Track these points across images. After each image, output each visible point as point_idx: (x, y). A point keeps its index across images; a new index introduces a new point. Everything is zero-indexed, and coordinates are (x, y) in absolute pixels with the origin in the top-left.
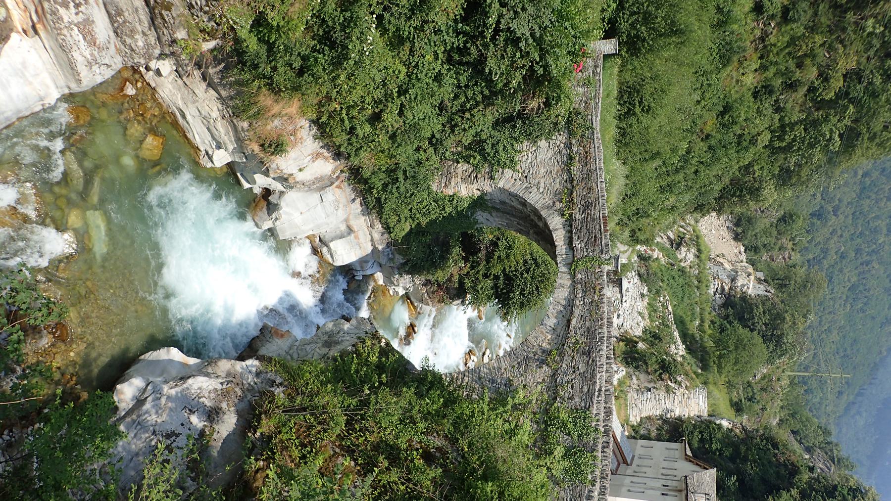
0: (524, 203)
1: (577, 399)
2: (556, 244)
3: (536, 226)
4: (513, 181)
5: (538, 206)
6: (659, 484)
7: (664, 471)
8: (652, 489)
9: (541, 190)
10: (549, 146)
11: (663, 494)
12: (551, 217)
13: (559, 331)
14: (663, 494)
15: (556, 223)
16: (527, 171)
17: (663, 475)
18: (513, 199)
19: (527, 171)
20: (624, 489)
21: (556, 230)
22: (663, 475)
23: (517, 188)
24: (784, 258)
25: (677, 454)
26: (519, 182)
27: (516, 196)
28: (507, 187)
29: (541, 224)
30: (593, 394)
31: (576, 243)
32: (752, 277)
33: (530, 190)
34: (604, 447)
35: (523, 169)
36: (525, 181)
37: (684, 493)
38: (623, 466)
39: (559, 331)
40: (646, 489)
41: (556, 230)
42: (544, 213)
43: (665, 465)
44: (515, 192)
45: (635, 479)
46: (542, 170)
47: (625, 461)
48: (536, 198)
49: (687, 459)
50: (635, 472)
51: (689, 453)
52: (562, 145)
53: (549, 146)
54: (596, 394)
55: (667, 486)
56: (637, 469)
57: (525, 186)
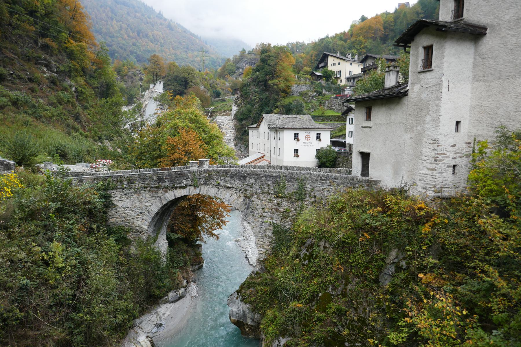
0: (157, 214)
1: (269, 183)
2: (183, 195)
3: (169, 207)
4: (143, 221)
5: (160, 206)
6: (274, 141)
7: (266, 138)
8: (277, 144)
9: (150, 204)
10: (122, 201)
11: (279, 139)
12: (167, 198)
13: (232, 193)
14: (279, 139)
15: (170, 195)
16: (137, 213)
17: (268, 139)
18: (154, 220)
19: (137, 213)
20: (279, 158)
21: (175, 195)
22: (268, 139)
23: (148, 219)
24: (139, 74)
25: (255, 132)
26: (145, 217)
27: (153, 219)
28: (147, 224)
29: (169, 204)
30: (266, 175)
31: (183, 185)
32: (153, 90)
33: (150, 210)
34: (287, 169)
35: (136, 215)
36: (144, 214)
37: (278, 129)
38: (265, 158)
39: (232, 193)
40: (277, 147)
41: (175, 195)
42: (165, 203)
43: (262, 137)
44: (151, 219)
45: (272, 152)
46: (137, 204)
47: (263, 157)
48: (155, 207)
49: (258, 127)
50: (268, 153)
51: (255, 126)
52: (121, 193)
53: (122, 201)
54: (265, 173)
55: (274, 137)
56: (266, 151)
57: (147, 214)
